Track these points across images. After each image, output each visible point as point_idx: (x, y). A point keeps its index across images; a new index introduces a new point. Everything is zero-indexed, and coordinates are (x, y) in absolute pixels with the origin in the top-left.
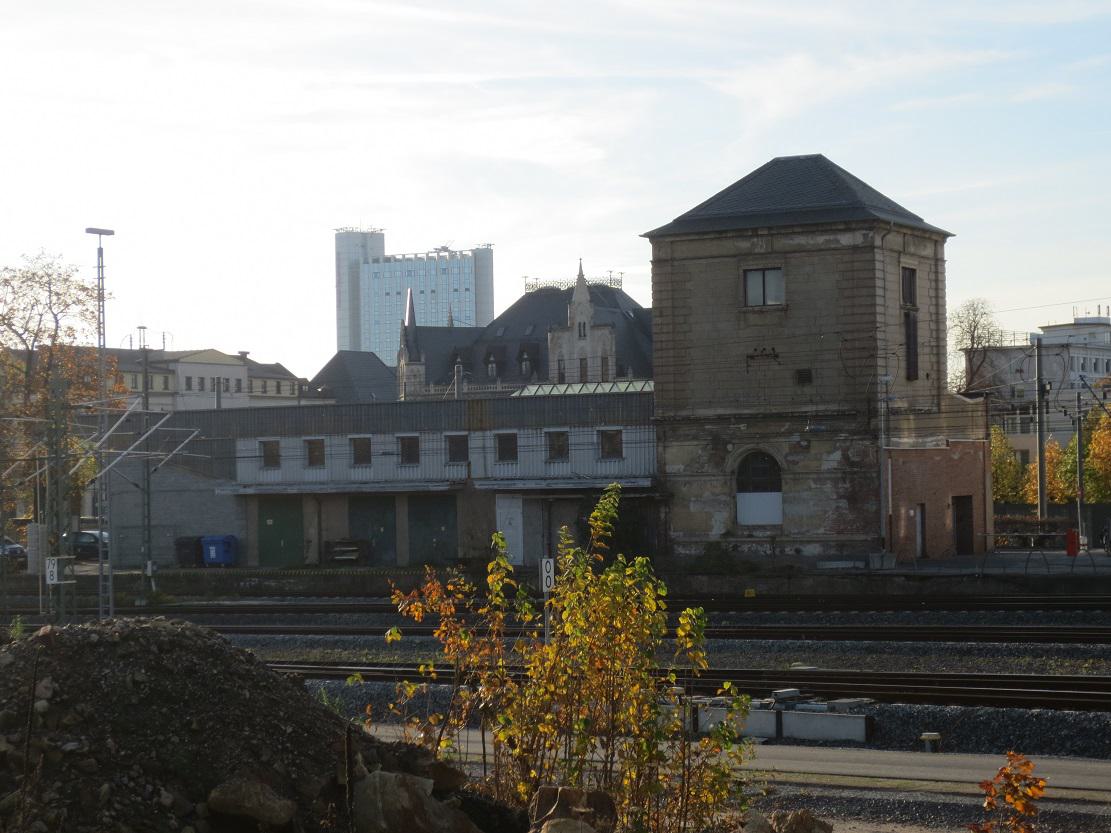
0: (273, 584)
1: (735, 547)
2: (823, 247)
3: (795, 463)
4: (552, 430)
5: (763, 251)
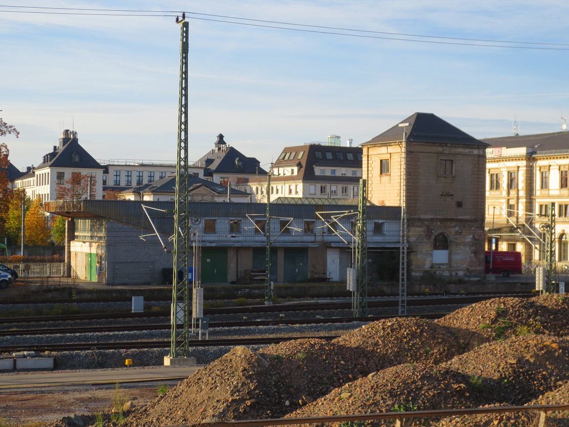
0: (257, 292)
1: (435, 272)
2: (468, 154)
3: (456, 239)
4: (307, 220)
5: (447, 152)
